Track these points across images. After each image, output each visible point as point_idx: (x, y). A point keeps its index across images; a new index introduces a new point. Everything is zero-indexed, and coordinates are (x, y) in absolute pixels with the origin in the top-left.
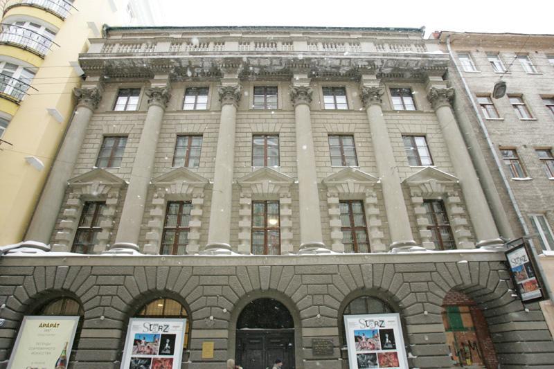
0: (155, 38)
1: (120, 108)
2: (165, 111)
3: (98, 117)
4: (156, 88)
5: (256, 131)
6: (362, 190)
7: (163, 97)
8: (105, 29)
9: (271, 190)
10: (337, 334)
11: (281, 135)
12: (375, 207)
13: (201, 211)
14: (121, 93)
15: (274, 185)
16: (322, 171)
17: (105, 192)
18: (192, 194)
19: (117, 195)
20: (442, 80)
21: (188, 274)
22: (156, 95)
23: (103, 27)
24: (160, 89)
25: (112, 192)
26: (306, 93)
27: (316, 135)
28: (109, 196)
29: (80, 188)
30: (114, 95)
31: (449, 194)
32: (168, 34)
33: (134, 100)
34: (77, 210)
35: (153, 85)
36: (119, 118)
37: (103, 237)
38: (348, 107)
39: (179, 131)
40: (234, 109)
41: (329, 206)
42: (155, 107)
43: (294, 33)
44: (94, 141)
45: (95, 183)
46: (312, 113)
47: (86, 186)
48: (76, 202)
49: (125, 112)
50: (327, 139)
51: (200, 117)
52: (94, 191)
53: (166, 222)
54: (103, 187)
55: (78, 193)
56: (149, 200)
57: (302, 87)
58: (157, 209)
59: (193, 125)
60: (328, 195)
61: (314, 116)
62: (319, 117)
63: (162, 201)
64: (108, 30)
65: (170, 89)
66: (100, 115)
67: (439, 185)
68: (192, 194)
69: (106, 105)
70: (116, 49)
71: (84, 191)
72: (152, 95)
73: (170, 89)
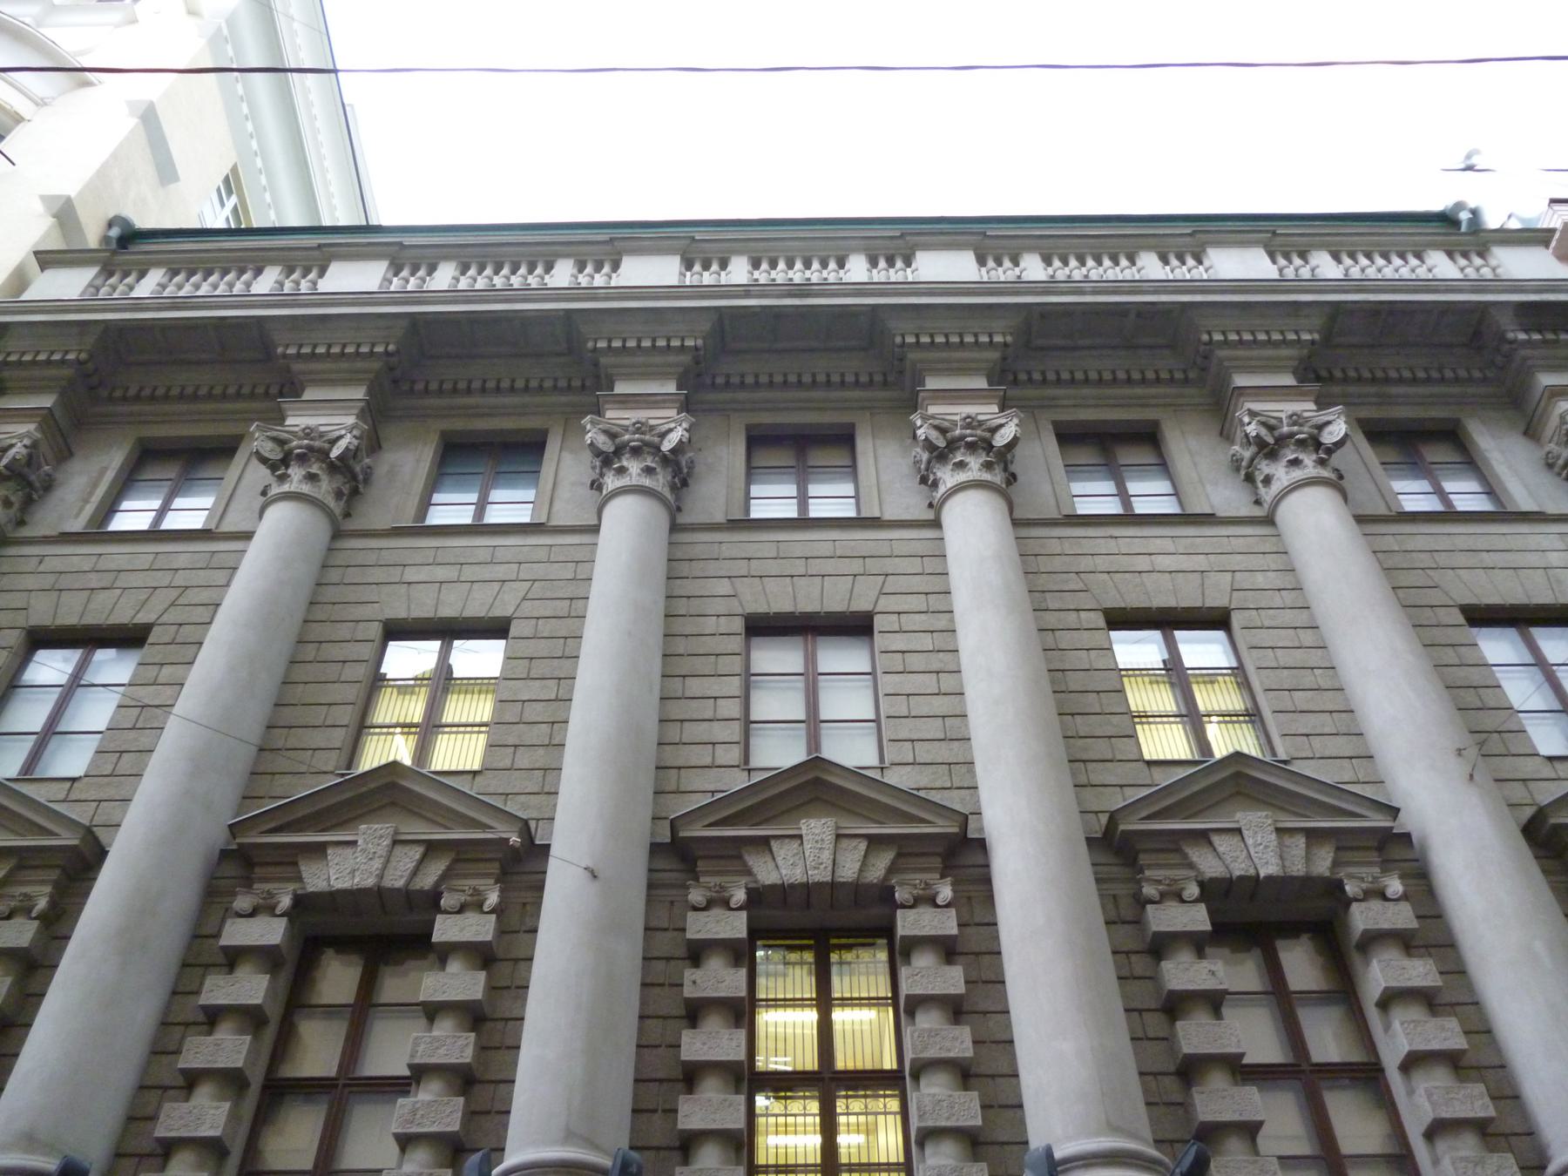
0: (320, 246)
4: (308, 432)
5: (402, 614)
6: (1323, 863)
7: (334, 468)
8: (115, 232)
9: (849, 870)
11: (879, 622)
12: (1200, 954)
13: (482, 976)
15: (863, 845)
16: (1095, 779)
19: (42, 904)
20: (1294, 383)
23: (110, 225)
24: (322, 435)
26: (988, 446)
27: (1051, 619)
28: (447, 901)
29: (290, 859)
30: (114, 459)
31: (1350, 888)
35: (297, 421)
38: (858, 510)
40: (661, 517)
41: (1160, 947)
42: (960, 498)
46: (1024, 532)
47: (319, 850)
50: (736, 643)
51: (500, 555)
54: (416, 853)
56: (206, 931)
57: (970, 422)
58: (455, 966)
60: (1149, 890)
61: (1034, 546)
62: (1055, 546)
63: (270, 932)
65: (373, 443)
66: (27, 550)
67: (1301, 841)
70: (147, 287)
71: (1208, 865)
73: (373, 443)
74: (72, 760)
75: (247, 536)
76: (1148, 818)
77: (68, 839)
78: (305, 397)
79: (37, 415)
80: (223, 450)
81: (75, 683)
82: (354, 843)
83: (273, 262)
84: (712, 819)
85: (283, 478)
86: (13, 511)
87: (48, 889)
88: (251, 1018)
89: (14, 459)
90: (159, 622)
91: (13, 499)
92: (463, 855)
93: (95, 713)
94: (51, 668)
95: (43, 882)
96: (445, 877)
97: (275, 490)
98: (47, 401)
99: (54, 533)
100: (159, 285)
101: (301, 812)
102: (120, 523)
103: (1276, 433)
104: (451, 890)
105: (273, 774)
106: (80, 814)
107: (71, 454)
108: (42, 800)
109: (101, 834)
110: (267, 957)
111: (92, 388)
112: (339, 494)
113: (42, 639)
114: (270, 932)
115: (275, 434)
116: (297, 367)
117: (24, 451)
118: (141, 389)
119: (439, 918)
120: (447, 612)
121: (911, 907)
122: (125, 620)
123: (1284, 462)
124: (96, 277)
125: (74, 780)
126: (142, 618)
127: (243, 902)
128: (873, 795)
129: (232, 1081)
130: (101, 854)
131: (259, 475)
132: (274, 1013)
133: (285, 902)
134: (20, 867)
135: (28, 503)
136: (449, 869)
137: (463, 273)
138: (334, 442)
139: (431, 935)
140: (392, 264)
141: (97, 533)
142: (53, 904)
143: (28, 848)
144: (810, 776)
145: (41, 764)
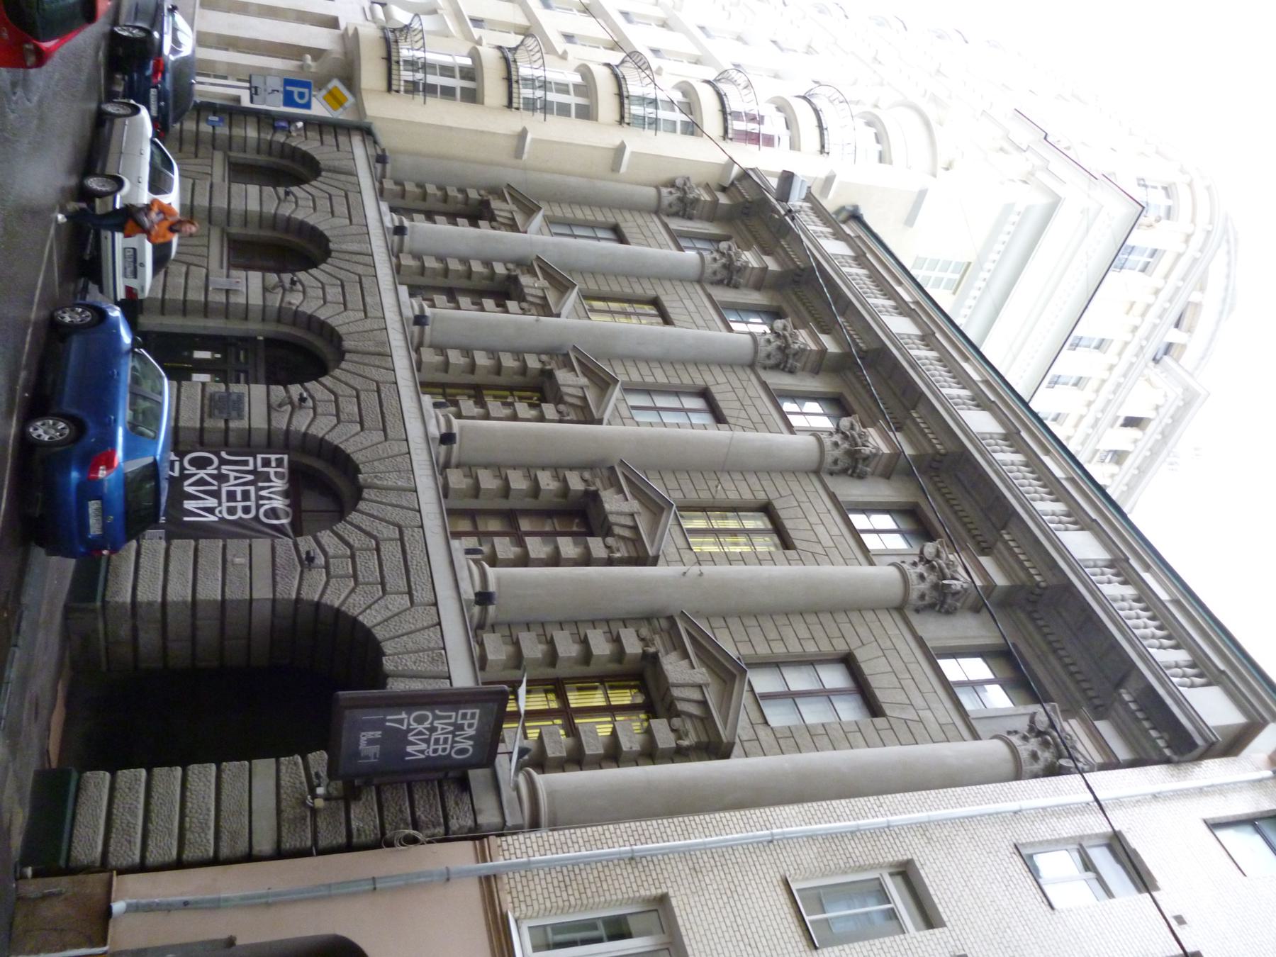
0: (1094, 521)
1: (953, 669)
2: (900, 609)
3: (892, 627)
10: (271, 762)
14: (1000, 656)
17: (617, 530)
18: (678, 714)
19: (685, 743)
21: (360, 269)
22: (1045, 744)
25: (689, 725)
28: (676, 722)
32: (967, 359)
33: (997, 698)
34: (556, 496)
36: (836, 526)
37: (499, 548)
39: (860, 655)
43: (1155, 575)
44: (819, 633)
45: (700, 674)
48: (633, 646)
49: (856, 534)
52: (613, 503)
53: (527, 513)
55: (658, 645)
59: (881, 654)
64: (855, 216)
68: (678, 714)
69: (936, 630)
72: (1040, 734)
74: (778, 716)
75: (976, 736)
76: (689, 633)
77: (725, 735)
78: (1098, 724)
79: (1108, 757)
80: (1035, 699)
81: (827, 694)
82: (693, 668)
83: (1026, 455)
84: (690, 630)
85: (1025, 738)
86: (920, 603)
87: (626, 555)
88: (587, 656)
89: (949, 585)
90: (800, 552)
91: (927, 598)
92: (706, 720)
93: (814, 713)
94: (834, 678)
95: (628, 552)
96: (690, 716)
97: (1015, 739)
98: (1000, 580)
99: (832, 490)
100: (1176, 662)
101: (550, 271)
102: (948, 666)
103: (861, 461)
104: (683, 721)
105: (728, 627)
106: (744, 730)
107: (817, 373)
108: (743, 701)
109: (737, 749)
110: (620, 654)
111: (931, 467)
112: (922, 597)
113: (848, 662)
114: (633, 646)
115: (941, 549)
116: (1000, 545)
117: (959, 588)
118: (1057, 641)
119: (599, 539)
120: (789, 524)
121: (638, 636)
122: (782, 516)
123: (927, 592)
124: (916, 335)
125: (766, 723)
126: (797, 543)
127: (644, 632)
128: (710, 648)
129: (552, 657)
130: (726, 754)
131: (1022, 725)
132: (593, 669)
133: (651, 650)
134: (633, 541)
135: (844, 472)
136: (696, 716)
137: (1135, 601)
138: (953, 578)
139: (510, 299)
140: (1111, 561)
141: (931, 657)
142: (688, 748)
143: (714, 721)
144: (663, 505)
145: (768, 702)
